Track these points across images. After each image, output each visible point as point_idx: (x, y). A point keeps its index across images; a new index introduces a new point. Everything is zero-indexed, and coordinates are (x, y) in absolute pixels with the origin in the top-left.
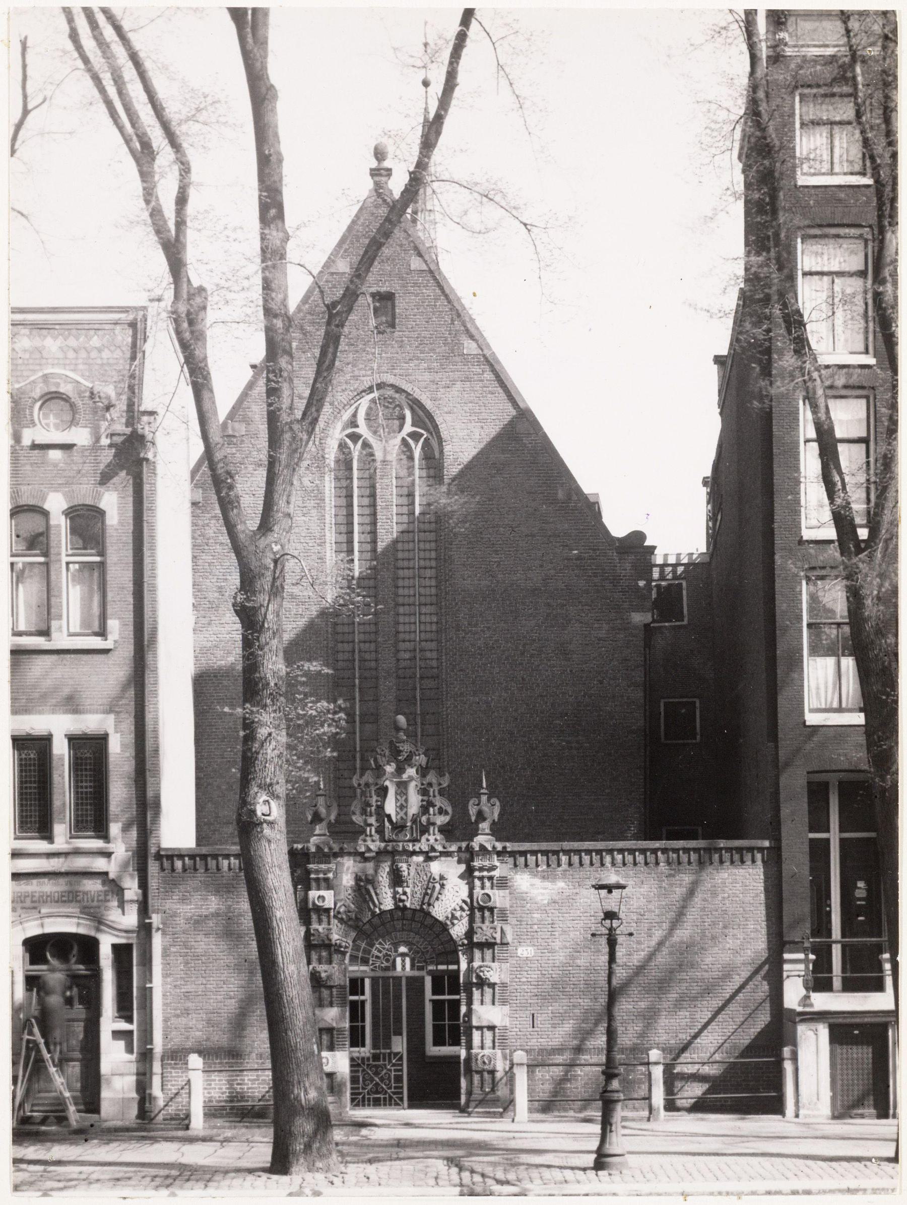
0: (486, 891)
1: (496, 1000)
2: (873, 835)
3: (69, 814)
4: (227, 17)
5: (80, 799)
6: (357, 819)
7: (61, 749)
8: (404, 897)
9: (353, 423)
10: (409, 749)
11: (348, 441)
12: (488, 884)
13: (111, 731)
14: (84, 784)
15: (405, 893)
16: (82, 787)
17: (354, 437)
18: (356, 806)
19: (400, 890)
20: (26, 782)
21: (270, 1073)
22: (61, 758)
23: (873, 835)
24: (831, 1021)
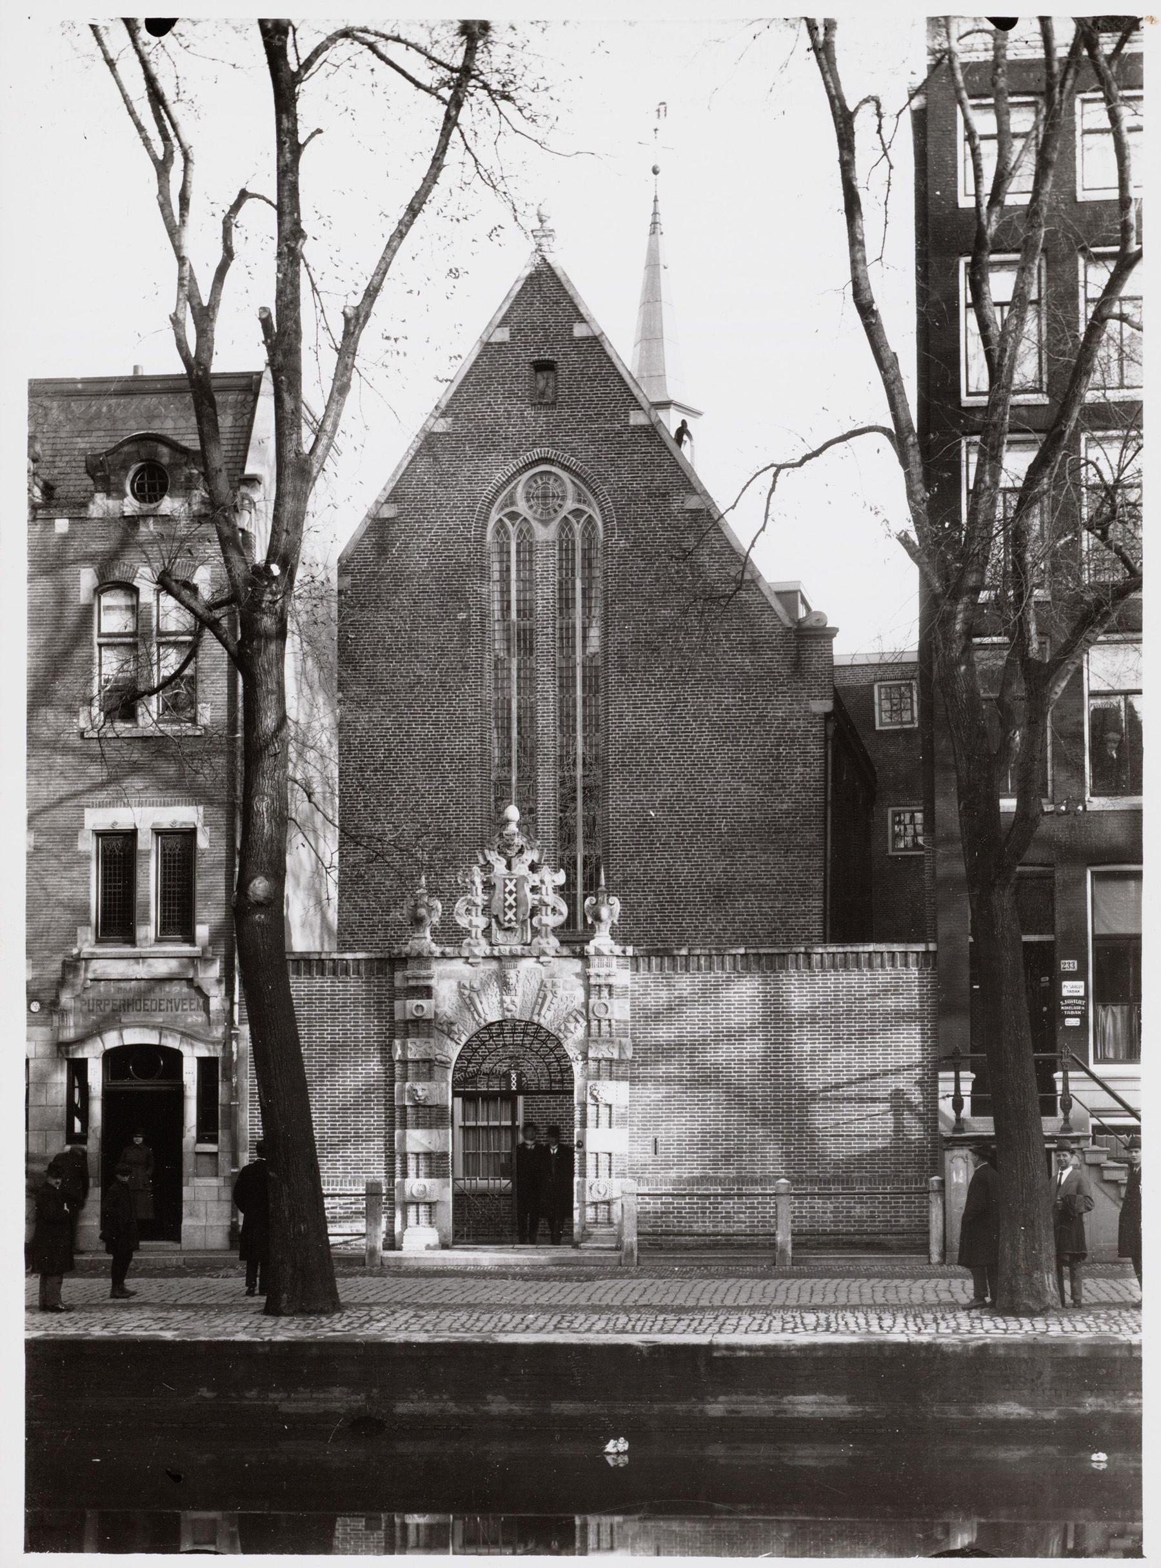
0: (603, 1001)
1: (614, 1122)
2: (1025, 938)
3: (154, 913)
4: (122, 25)
5: (166, 896)
6: (463, 922)
7: (146, 842)
8: (511, 1007)
9: (511, 500)
10: (521, 843)
11: (506, 520)
12: (605, 993)
13: (199, 826)
14: (172, 883)
15: (513, 1002)
16: (110, 887)
17: (513, 516)
18: (460, 906)
19: (507, 999)
20: (110, 881)
21: (326, 1206)
22: (147, 853)
23: (1025, 938)
24: (177, 1247)
